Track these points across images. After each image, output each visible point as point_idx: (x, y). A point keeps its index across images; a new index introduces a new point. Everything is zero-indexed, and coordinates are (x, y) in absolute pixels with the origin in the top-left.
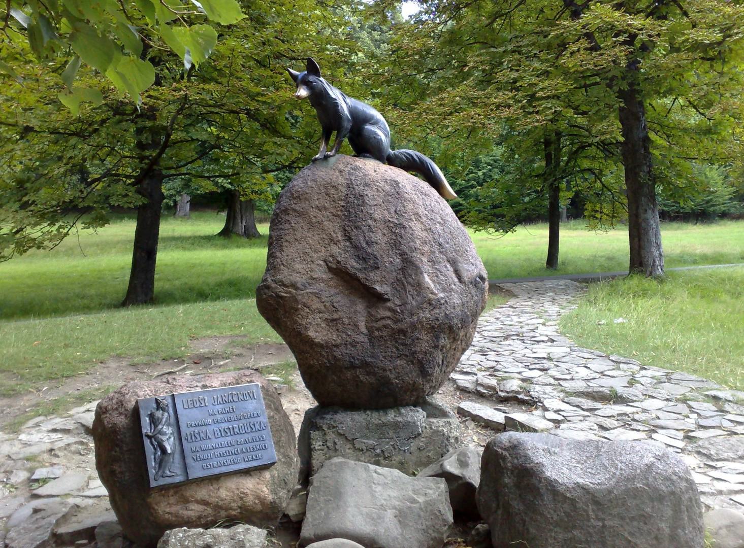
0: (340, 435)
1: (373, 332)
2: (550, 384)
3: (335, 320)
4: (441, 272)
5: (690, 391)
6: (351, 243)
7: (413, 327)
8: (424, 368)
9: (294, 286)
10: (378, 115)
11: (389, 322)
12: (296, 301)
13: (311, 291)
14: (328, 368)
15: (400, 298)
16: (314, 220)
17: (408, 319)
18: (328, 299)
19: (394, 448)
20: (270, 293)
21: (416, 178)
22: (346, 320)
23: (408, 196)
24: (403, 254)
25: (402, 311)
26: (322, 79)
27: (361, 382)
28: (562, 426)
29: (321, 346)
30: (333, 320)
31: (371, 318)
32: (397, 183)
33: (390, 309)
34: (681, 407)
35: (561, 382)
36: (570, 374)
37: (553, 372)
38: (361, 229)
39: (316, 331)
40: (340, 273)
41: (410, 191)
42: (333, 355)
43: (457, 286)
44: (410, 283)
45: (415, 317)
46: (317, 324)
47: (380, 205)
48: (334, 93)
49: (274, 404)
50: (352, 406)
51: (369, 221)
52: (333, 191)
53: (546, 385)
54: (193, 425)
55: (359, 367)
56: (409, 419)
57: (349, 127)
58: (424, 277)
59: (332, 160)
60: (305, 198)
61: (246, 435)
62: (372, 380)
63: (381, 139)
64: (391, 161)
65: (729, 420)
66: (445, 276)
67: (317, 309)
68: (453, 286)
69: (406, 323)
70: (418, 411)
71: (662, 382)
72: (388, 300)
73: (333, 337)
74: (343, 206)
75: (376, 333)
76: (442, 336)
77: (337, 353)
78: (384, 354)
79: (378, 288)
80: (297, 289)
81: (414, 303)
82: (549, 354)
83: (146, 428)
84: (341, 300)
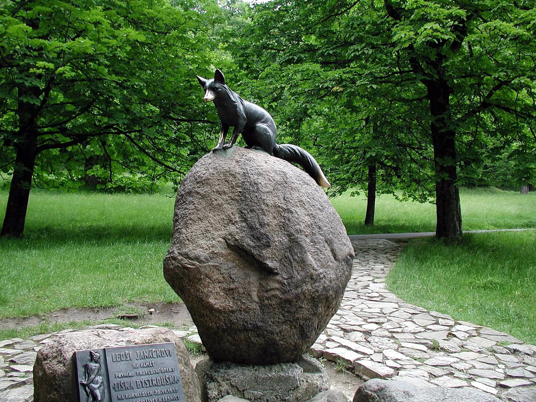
0: (232, 386)
1: (264, 301)
2: (385, 336)
3: (232, 289)
4: (321, 251)
5: (496, 345)
6: (247, 224)
7: (297, 297)
8: (304, 331)
9: (197, 259)
10: (267, 115)
11: (277, 293)
12: (200, 272)
13: (212, 264)
14: (224, 330)
15: (287, 272)
16: (215, 203)
17: (293, 291)
18: (226, 272)
19: (277, 398)
20: (177, 264)
21: (298, 169)
22: (241, 290)
23: (294, 186)
24: (290, 235)
25: (288, 283)
26: (225, 86)
27: (252, 343)
28: (401, 373)
29: (220, 311)
30: (230, 290)
31: (263, 289)
32: (285, 174)
33: (279, 282)
34: (492, 359)
35: (394, 335)
36: (400, 327)
37: (387, 326)
38: (255, 212)
39: (216, 299)
40: (238, 250)
41: (296, 181)
42: (229, 319)
43: (333, 264)
44: (296, 260)
45: (300, 289)
46: (216, 293)
47: (272, 192)
48: (235, 96)
49: (184, 358)
50: (243, 362)
51: (263, 206)
52: (231, 179)
53: (383, 337)
54: (120, 376)
55: (251, 330)
56: (290, 375)
57: (244, 124)
58: (307, 256)
59: (230, 151)
60: (207, 183)
61: (162, 386)
62: (261, 341)
63: (270, 135)
64: (277, 153)
65: (530, 371)
66: (324, 254)
67: (217, 279)
68: (330, 263)
69: (292, 294)
70: (296, 367)
71: (473, 336)
72: (277, 274)
73: (230, 304)
74: (240, 192)
75: (266, 301)
76: (320, 305)
77: (233, 318)
78: (272, 320)
79: (270, 264)
80: (200, 261)
81: (299, 277)
82: (382, 309)
83: (82, 380)
84: (237, 273)
